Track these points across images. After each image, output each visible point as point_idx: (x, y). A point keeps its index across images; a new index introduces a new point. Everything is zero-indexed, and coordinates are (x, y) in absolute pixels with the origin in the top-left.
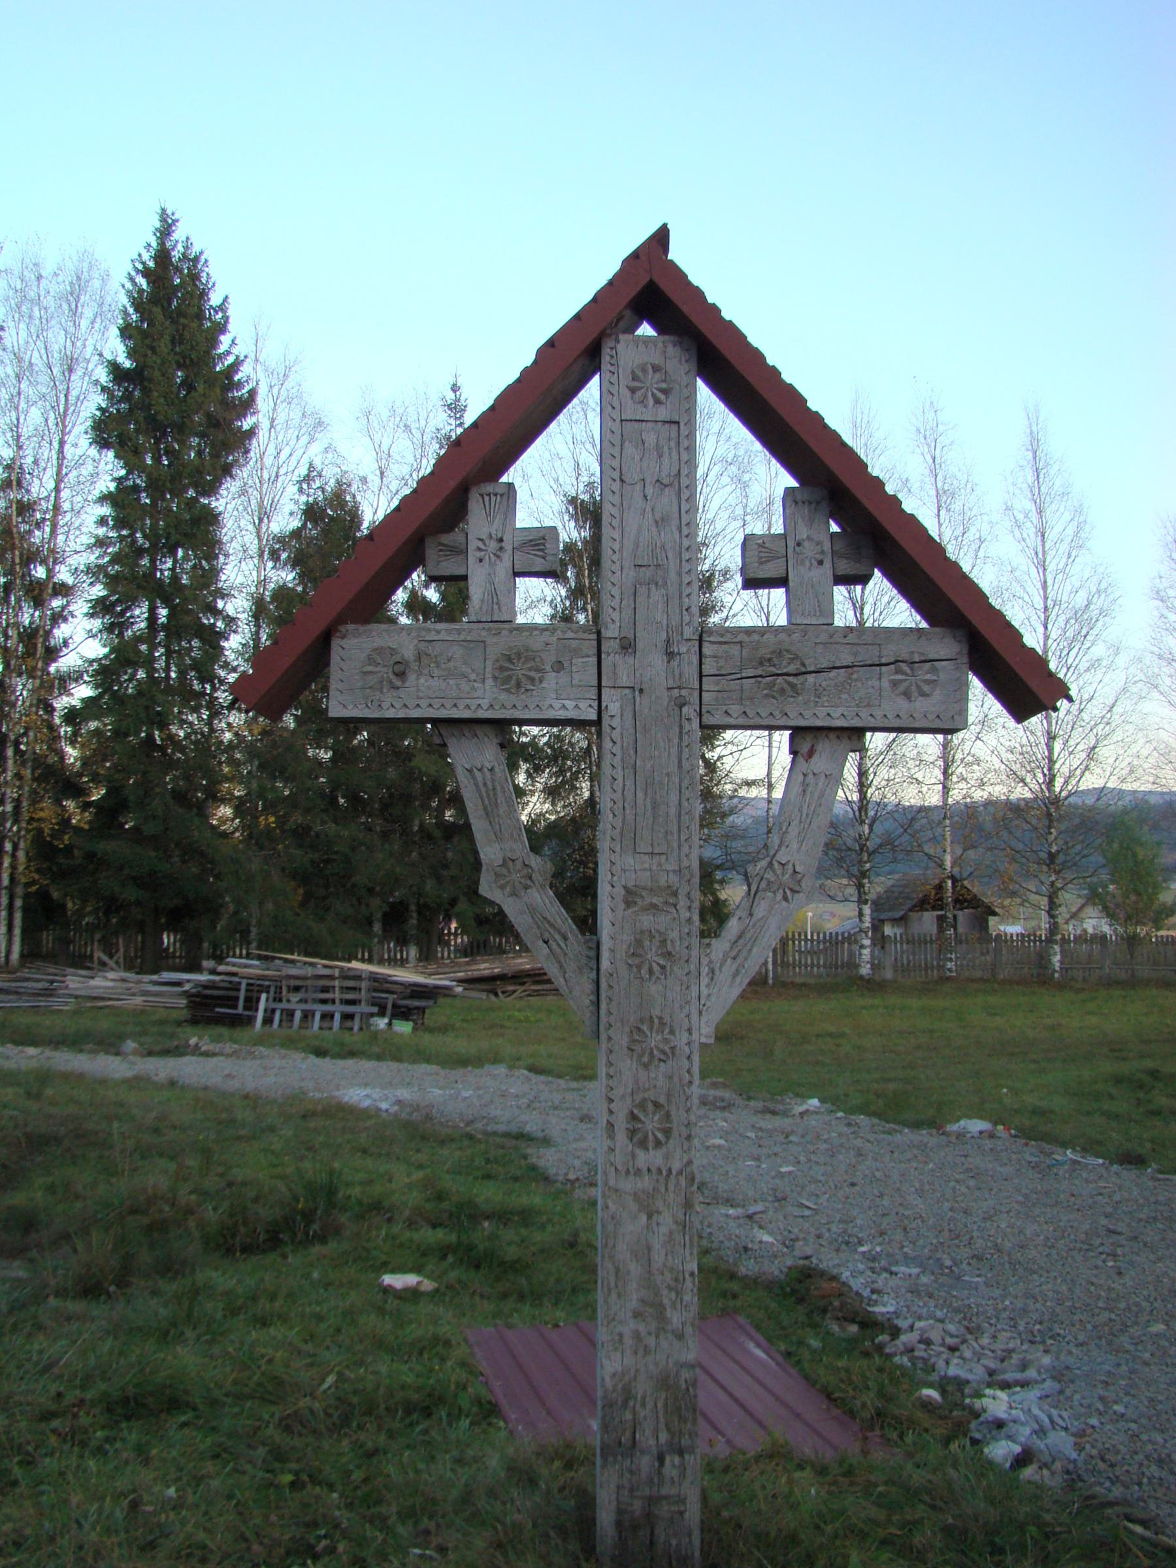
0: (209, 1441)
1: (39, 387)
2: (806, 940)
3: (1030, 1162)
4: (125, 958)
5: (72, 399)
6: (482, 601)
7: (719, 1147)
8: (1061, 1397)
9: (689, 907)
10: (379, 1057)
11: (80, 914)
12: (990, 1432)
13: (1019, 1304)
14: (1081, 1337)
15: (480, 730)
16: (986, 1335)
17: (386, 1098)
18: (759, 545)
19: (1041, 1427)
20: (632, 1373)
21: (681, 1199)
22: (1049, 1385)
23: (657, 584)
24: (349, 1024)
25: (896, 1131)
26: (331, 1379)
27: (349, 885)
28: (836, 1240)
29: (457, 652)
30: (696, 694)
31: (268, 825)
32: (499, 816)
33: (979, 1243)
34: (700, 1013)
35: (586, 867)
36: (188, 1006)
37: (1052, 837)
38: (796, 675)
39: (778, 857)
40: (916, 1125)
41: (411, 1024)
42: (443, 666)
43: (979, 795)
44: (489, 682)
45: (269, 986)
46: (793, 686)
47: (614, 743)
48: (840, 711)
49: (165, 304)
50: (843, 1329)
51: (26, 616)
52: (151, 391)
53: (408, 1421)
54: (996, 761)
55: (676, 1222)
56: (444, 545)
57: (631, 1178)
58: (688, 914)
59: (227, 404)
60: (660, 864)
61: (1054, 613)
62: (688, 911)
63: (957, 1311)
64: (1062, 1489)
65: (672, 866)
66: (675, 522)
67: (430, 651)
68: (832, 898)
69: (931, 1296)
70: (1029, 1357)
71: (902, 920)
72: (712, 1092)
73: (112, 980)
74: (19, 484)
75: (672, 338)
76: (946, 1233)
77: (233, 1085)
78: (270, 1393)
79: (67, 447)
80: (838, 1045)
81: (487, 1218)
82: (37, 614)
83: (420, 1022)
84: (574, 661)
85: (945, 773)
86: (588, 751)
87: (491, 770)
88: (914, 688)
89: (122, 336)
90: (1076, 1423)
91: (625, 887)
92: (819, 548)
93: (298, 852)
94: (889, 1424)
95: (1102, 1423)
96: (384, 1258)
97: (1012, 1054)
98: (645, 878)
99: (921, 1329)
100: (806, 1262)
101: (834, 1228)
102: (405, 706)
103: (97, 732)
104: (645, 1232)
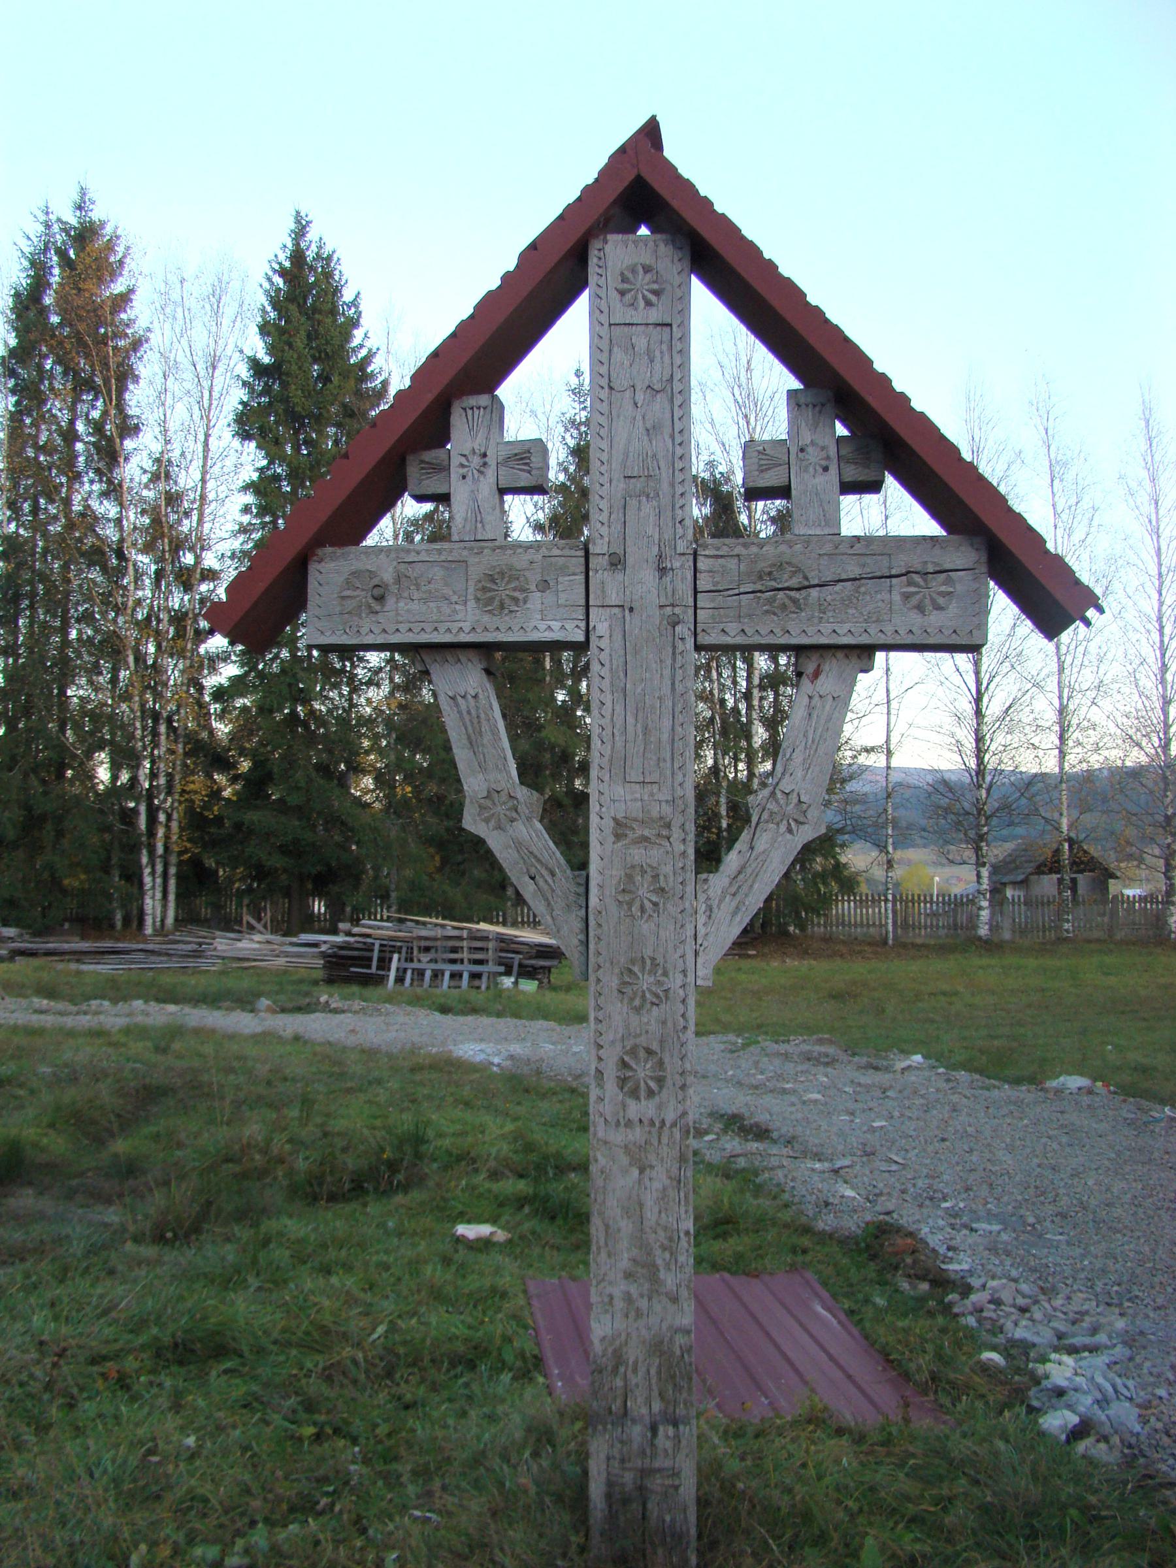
0: (244, 1389)
1: (184, 384)
2: (931, 902)
3: (1126, 1119)
4: (272, 921)
5: (216, 395)
6: (466, 520)
7: (816, 1101)
8: (1131, 1364)
9: (684, 840)
10: (499, 1015)
11: (230, 881)
12: (1050, 1401)
13: (1098, 1264)
14: (1160, 1301)
15: (463, 655)
16: (1060, 1296)
17: (499, 1053)
18: (759, 452)
19: (1104, 1395)
20: (623, 1337)
21: (675, 1153)
22: (1120, 1351)
23: (648, 496)
24: (476, 983)
25: (995, 1087)
26: (381, 1329)
27: (482, 852)
28: (920, 1195)
29: (438, 573)
30: (691, 611)
31: (404, 795)
32: (483, 745)
33: (1064, 1201)
34: (696, 953)
35: (709, 831)
36: (324, 967)
37: (1168, 800)
38: (798, 589)
39: (781, 786)
40: (1017, 1081)
41: (536, 982)
42: (424, 588)
43: (1096, 761)
44: (471, 604)
45: (401, 947)
46: (795, 601)
47: (603, 665)
48: (847, 626)
49: (301, 302)
50: (914, 1287)
51: (176, 600)
52: (288, 384)
53: (452, 1373)
54: (1111, 726)
55: (670, 1178)
56: (428, 463)
57: (622, 1129)
58: (682, 847)
59: (359, 394)
60: (652, 794)
61: (1169, 579)
62: (683, 843)
63: (1033, 1270)
64: (1118, 1465)
65: (665, 796)
66: (667, 431)
67: (410, 574)
68: (952, 862)
69: (1008, 1254)
70: (1103, 1320)
71: (1024, 883)
72: (817, 1048)
73: (259, 942)
74: (168, 476)
75: (664, 236)
76: (1032, 1191)
77: (351, 1041)
78: (316, 1342)
79: (211, 440)
80: (950, 1004)
81: (574, 1169)
82: (187, 598)
83: (546, 981)
84: (560, 579)
85: (1062, 738)
86: (712, 719)
87: (475, 697)
88: (927, 601)
89: (261, 334)
90: (1142, 1393)
91: (614, 819)
92: (823, 454)
93: (430, 819)
94: (944, 1389)
95: (1170, 1394)
96: (460, 1207)
97: (1123, 1013)
98: (635, 810)
99: (992, 1288)
100: (887, 1218)
101: (920, 1183)
102: (384, 631)
103: (245, 709)
104: (636, 1187)
